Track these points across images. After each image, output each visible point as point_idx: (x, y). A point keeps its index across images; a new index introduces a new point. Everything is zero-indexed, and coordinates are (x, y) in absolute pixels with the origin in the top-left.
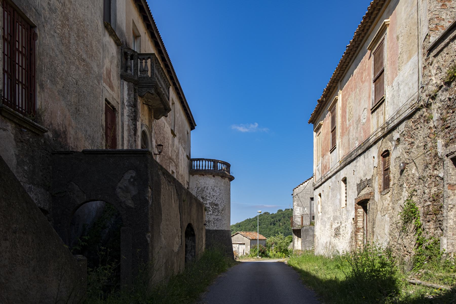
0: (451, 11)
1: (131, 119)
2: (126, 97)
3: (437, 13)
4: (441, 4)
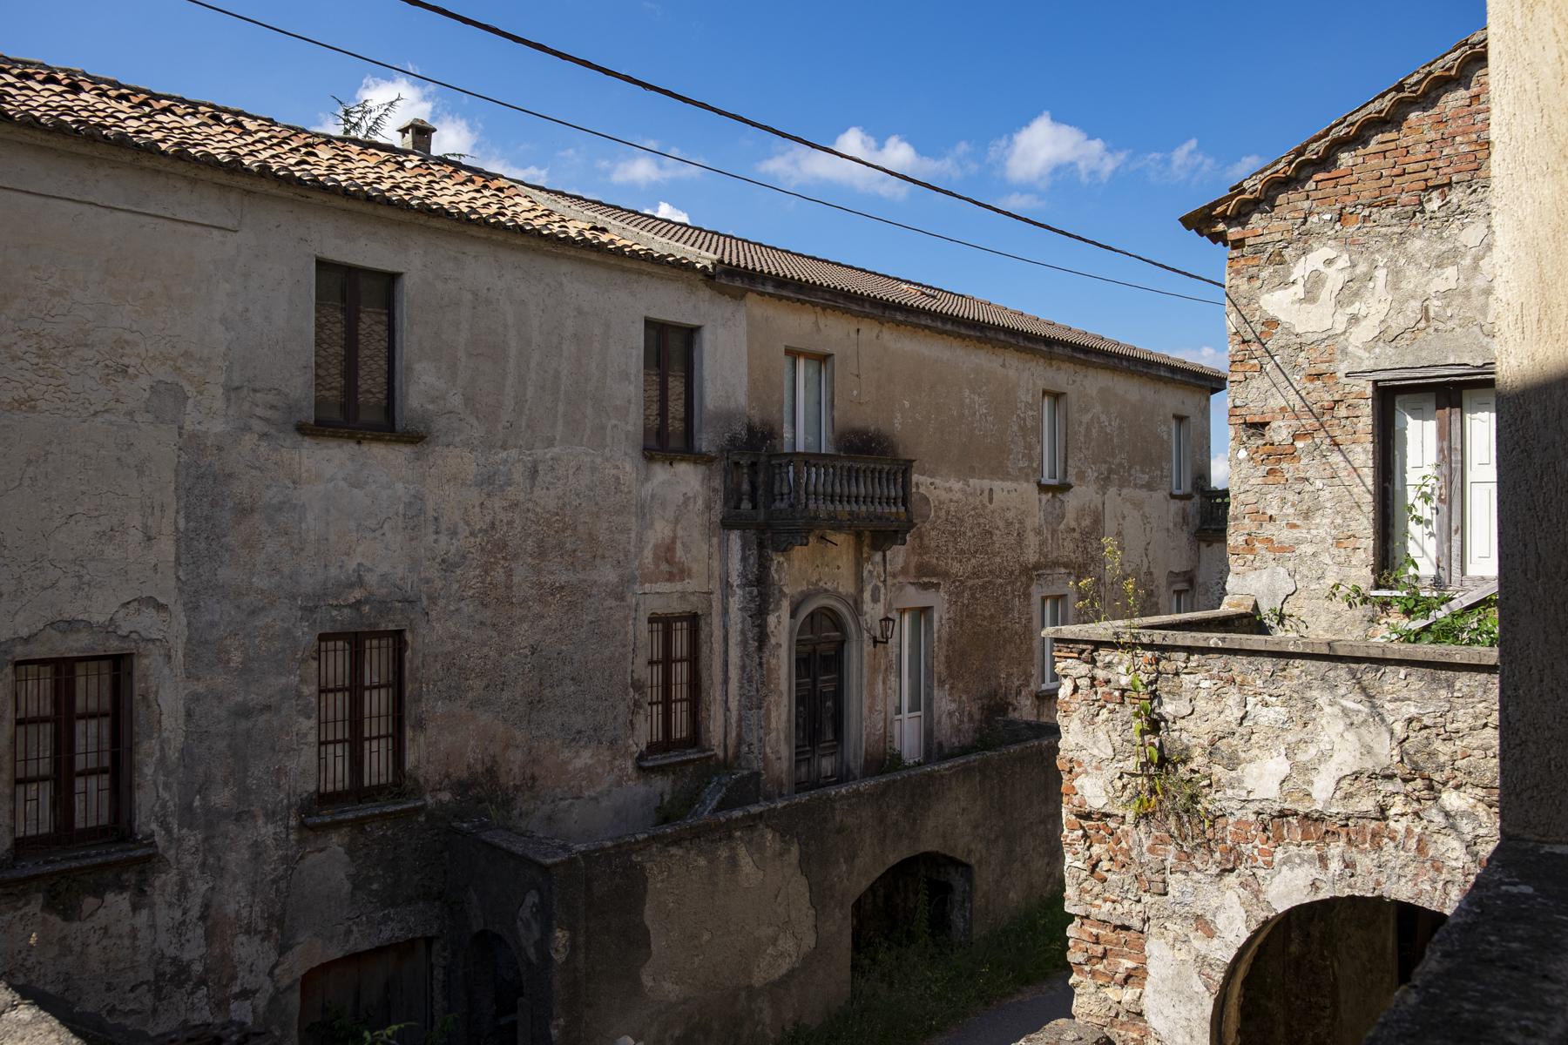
0: (1297, 491)
1: (750, 616)
2: (735, 565)
3: (1251, 498)
4: (1264, 469)
